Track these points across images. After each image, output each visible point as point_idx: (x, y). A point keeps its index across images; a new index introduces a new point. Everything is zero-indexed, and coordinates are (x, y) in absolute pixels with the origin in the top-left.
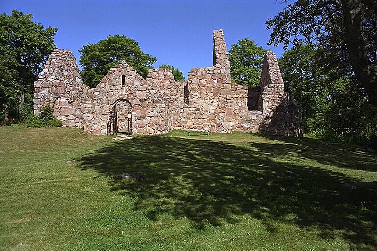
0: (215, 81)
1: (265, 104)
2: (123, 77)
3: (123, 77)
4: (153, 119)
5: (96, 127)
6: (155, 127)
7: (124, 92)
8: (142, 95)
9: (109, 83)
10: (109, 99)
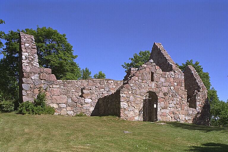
0: (176, 84)
1: (198, 103)
2: (152, 73)
3: (152, 73)
4: (172, 109)
5: (131, 114)
6: (173, 115)
7: (153, 86)
8: (165, 90)
9: (141, 77)
10: (141, 91)
